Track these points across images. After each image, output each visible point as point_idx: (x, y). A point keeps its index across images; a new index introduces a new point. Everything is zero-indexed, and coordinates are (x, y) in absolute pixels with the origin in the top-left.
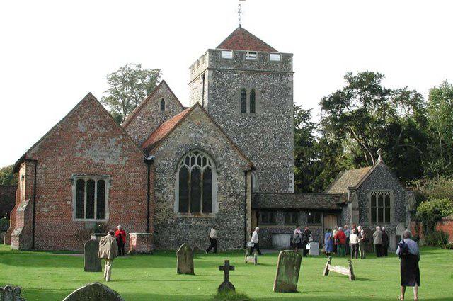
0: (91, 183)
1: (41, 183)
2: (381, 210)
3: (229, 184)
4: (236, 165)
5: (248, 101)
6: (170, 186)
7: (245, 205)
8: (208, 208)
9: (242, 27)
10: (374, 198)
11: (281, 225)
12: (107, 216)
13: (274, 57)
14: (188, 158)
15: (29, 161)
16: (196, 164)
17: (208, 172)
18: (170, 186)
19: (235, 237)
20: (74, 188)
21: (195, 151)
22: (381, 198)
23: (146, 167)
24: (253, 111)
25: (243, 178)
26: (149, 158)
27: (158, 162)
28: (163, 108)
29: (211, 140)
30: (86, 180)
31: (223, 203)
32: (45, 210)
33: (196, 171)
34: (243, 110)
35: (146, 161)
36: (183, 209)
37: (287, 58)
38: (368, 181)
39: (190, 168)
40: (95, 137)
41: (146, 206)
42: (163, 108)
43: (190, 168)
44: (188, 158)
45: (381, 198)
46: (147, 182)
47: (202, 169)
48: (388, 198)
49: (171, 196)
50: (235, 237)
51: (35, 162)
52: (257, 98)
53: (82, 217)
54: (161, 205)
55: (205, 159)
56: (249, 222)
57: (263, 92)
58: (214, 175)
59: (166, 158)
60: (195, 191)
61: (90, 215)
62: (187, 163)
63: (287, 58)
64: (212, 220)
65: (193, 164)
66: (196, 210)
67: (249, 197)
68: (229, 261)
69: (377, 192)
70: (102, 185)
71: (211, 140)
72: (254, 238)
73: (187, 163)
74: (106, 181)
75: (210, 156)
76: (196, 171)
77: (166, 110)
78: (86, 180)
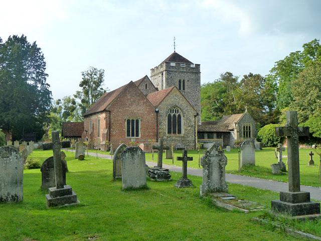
0: (133, 121)
1: (112, 121)
2: (247, 132)
3: (188, 121)
4: (192, 113)
5: (182, 85)
6: (164, 122)
7: (195, 130)
8: (180, 132)
9: (36, 43)
10: (244, 127)
11: (206, 139)
12: (140, 135)
13: (192, 66)
14: (171, 110)
15: (107, 111)
16: (174, 112)
17: (179, 116)
18: (164, 122)
19: (191, 144)
20: (126, 123)
21: (174, 108)
22: (247, 127)
23: (155, 114)
24: (184, 89)
25: (194, 119)
26: (157, 110)
27: (160, 112)
28: (146, 88)
29: (181, 102)
30: (131, 120)
31: (186, 130)
32: (114, 133)
33: (174, 115)
34: (180, 88)
35: (156, 111)
36: (169, 132)
37: (198, 66)
38: (241, 120)
39: (172, 114)
40: (134, 101)
41: (156, 131)
42: (146, 88)
43: (172, 114)
44: (171, 110)
45: (247, 127)
46: (156, 120)
47: (177, 115)
48: (250, 127)
49: (164, 127)
50: (191, 144)
51: (110, 112)
52: (186, 84)
53: (129, 136)
54: (160, 131)
55: (178, 110)
56: (196, 138)
57: (188, 81)
58: (182, 118)
59: (163, 112)
60: (174, 124)
61: (133, 135)
62: (171, 112)
63: (198, 66)
64: (182, 137)
65: (173, 112)
66: (175, 132)
67: (196, 127)
68: (284, 151)
69: (246, 125)
70: (137, 121)
71: (181, 102)
72: (198, 145)
73: (171, 112)
74: (140, 120)
75: (180, 109)
76: (174, 115)
77: (148, 88)
78: (131, 120)
